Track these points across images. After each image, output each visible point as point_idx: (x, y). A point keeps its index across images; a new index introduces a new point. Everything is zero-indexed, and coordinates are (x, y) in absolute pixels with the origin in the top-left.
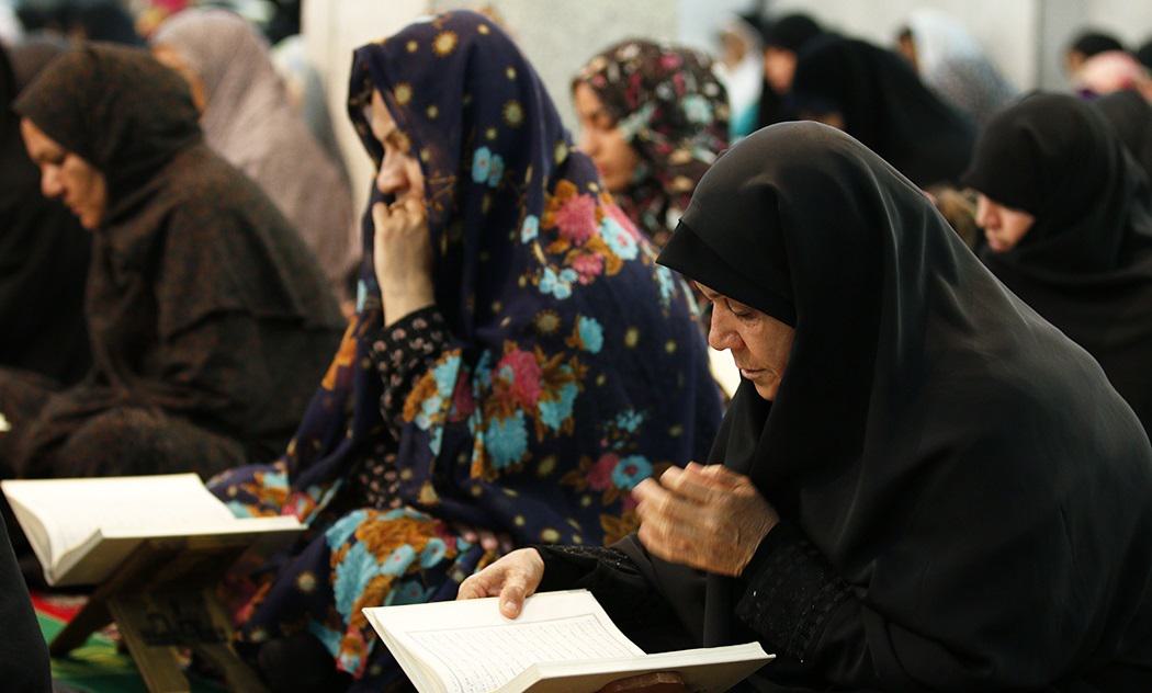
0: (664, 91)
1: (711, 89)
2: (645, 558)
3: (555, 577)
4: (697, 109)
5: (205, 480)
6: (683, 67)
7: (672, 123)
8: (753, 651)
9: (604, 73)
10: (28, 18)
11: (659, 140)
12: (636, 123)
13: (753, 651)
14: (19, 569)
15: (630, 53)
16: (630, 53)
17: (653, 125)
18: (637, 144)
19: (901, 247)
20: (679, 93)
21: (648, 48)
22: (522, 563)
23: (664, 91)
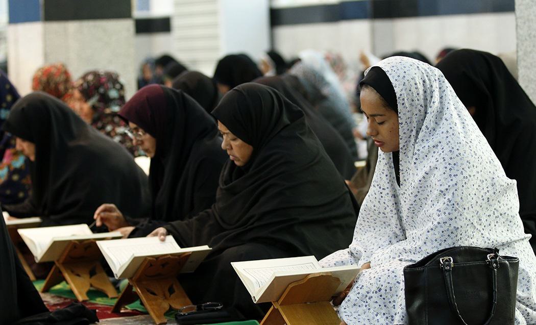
0: (102, 90)
1: (118, 86)
2: (383, 117)
3: (169, 233)
4: (113, 94)
5: (89, 225)
6: (108, 81)
7: (106, 100)
8: (206, 248)
9: (82, 85)
10: (177, 4)
11: (101, 105)
12: (94, 100)
13: (206, 248)
14: (235, 182)
15: (90, 78)
16: (90, 78)
17: (99, 101)
18: (94, 108)
19: (221, 105)
20: (107, 89)
21: (96, 74)
22: (162, 230)
23: (102, 90)
